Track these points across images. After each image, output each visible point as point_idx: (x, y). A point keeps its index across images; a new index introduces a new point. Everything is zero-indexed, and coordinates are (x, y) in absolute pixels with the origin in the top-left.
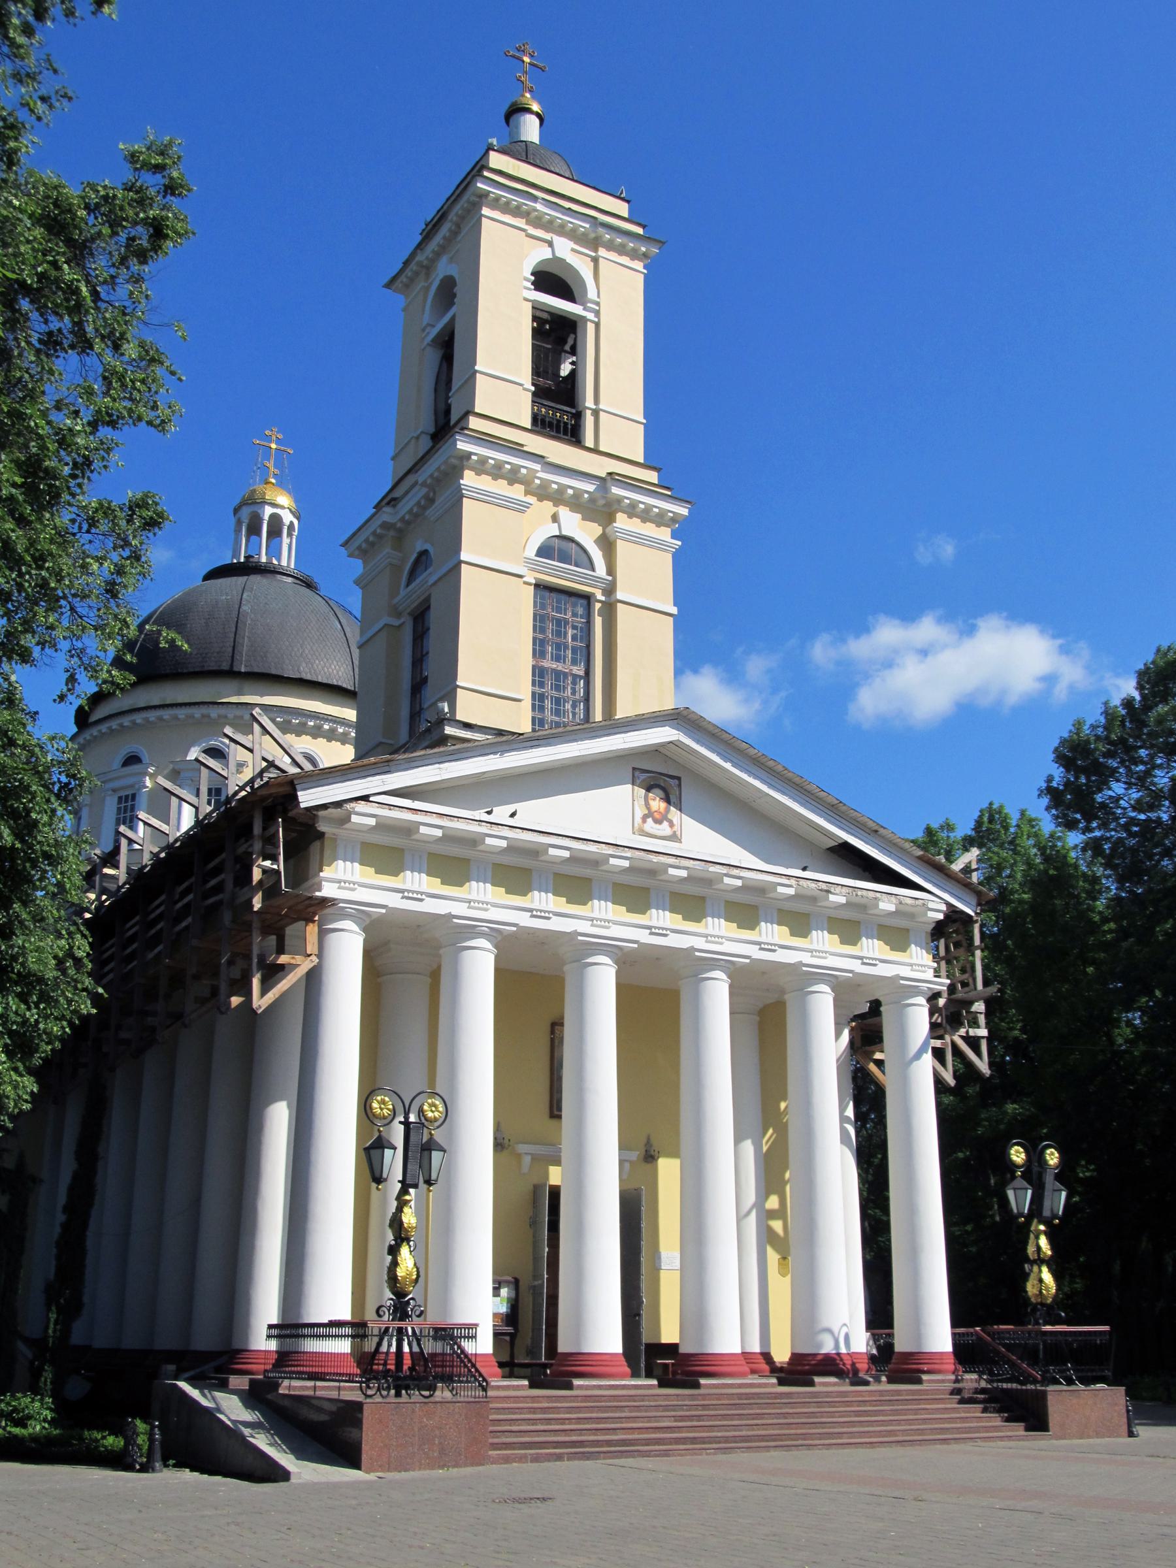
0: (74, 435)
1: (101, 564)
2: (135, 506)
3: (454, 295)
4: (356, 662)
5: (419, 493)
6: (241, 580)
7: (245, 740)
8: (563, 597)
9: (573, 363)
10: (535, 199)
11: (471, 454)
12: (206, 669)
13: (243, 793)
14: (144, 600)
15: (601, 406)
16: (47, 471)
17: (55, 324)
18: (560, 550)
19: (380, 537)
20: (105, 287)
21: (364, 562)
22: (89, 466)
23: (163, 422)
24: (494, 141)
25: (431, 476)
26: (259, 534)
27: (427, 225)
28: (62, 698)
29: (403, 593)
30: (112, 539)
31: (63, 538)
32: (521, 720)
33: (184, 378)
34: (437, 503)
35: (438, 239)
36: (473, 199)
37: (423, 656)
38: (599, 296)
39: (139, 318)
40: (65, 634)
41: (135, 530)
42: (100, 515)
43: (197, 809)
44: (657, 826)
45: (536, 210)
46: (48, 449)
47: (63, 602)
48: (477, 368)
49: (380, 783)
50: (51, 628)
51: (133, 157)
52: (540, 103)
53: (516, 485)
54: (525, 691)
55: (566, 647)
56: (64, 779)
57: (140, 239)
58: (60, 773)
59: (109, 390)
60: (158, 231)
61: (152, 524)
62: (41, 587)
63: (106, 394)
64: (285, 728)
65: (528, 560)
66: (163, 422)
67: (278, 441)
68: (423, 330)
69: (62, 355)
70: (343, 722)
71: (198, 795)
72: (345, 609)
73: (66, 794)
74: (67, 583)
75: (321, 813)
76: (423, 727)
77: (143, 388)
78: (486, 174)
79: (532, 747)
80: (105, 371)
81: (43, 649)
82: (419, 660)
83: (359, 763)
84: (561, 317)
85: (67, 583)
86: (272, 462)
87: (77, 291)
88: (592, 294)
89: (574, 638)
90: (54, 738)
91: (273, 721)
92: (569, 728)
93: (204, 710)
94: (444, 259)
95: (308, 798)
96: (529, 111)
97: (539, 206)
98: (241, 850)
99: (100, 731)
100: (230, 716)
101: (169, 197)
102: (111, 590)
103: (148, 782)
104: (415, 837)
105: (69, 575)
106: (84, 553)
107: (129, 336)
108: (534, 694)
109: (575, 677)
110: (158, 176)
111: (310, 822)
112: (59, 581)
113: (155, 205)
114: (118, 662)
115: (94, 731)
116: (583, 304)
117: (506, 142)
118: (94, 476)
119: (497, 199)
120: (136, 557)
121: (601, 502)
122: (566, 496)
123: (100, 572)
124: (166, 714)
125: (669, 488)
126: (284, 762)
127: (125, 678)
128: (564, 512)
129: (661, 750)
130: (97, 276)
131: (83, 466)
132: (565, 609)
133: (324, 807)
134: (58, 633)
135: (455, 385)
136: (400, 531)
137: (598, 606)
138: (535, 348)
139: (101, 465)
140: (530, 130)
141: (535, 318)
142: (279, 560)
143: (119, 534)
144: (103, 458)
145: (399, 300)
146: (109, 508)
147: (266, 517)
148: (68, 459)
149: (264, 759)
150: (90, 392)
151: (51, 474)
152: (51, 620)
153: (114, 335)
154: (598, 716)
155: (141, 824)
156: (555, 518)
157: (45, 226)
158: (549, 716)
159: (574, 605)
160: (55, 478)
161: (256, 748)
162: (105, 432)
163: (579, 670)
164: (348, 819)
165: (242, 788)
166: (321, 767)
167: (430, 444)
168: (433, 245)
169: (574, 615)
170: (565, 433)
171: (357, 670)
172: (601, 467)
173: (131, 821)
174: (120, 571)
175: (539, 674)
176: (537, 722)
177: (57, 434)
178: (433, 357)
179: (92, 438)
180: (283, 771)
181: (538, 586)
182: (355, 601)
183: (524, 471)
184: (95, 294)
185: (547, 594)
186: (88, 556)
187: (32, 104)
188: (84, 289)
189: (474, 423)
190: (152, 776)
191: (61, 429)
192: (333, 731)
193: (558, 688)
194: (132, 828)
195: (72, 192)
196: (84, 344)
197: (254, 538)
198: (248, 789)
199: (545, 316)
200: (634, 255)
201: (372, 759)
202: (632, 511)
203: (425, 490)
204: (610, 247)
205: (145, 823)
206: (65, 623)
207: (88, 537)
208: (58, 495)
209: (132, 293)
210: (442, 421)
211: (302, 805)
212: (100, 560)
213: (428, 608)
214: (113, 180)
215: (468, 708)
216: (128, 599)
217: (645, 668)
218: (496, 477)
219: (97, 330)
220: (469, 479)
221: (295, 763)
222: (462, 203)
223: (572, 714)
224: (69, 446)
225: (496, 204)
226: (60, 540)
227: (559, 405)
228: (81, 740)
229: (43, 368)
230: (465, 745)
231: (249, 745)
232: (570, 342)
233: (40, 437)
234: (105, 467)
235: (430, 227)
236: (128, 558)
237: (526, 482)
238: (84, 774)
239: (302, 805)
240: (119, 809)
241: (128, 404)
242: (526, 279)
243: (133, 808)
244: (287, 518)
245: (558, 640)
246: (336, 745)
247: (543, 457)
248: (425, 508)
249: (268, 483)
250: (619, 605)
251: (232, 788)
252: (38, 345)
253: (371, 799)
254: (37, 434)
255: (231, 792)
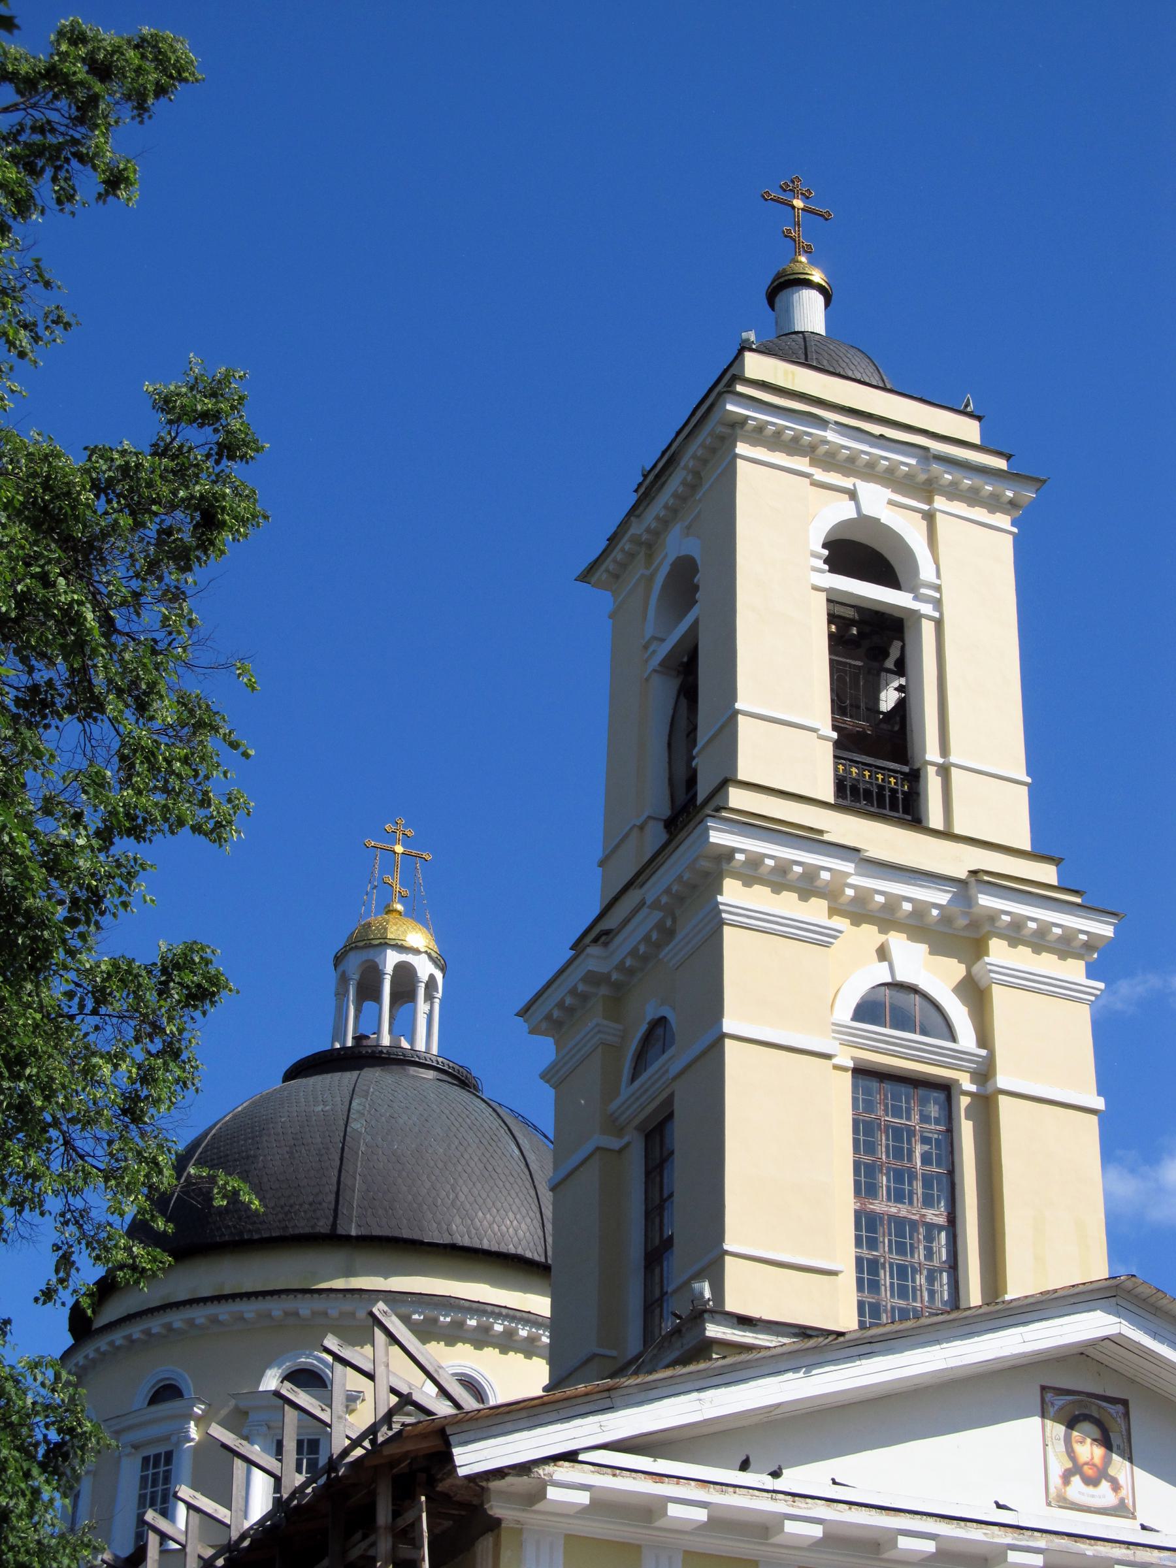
0: (73, 853)
1: (116, 1066)
2: (171, 967)
3: (696, 588)
4: (548, 1213)
5: (645, 923)
6: (349, 1077)
7: (360, 1355)
8: (903, 1089)
9: (900, 689)
10: (823, 423)
11: (733, 851)
12: (291, 1231)
13: (359, 1452)
14: (185, 1118)
15: (953, 759)
16: (28, 915)
17: (42, 675)
18: (893, 1008)
19: (584, 998)
20: (123, 610)
21: (557, 1043)
22: (97, 904)
23: (219, 825)
24: (751, 336)
25: (668, 891)
26: (378, 998)
27: (645, 476)
28: (48, 1295)
29: (626, 1091)
30: (132, 1023)
31: (54, 1024)
32: (839, 1310)
33: (252, 752)
34: (677, 940)
35: (665, 497)
36: (721, 429)
37: (663, 1201)
38: (938, 576)
39: (179, 658)
40: (57, 1186)
41: (171, 1009)
42: (114, 984)
43: (278, 1480)
44: (1091, 1490)
45: (826, 442)
46: (31, 880)
47: (53, 1133)
48: (738, 706)
49: (596, 1428)
50: (34, 1176)
51: (166, 403)
52: (825, 271)
53: (813, 900)
54: (842, 1253)
55: (912, 1176)
56: (54, 1436)
57: (179, 530)
58: (47, 1426)
59: (130, 777)
60: (209, 518)
61: (200, 996)
62: (19, 1109)
63: (126, 782)
64: (425, 1333)
65: (838, 1028)
66: (219, 825)
67: (407, 841)
68: (646, 647)
69: (54, 722)
70: (528, 1318)
71: (279, 1451)
72: (526, 1122)
73: (56, 1460)
74: (61, 1100)
75: (495, 1485)
76: (668, 1325)
77: (186, 771)
78: (740, 388)
79: (860, 1356)
80: (123, 745)
81: (20, 1212)
82: (657, 1206)
83: (558, 1394)
84: (877, 613)
85: (61, 1100)
86: (398, 876)
87: (76, 620)
88: (926, 572)
89: (926, 1159)
90: (37, 1365)
91: (406, 1320)
92: (924, 1321)
93: (288, 1303)
94: (676, 530)
95: (471, 1458)
96: (808, 284)
97: (831, 436)
98: (355, 1553)
99: (112, 1344)
100: (333, 1313)
101: (225, 461)
102: (132, 1110)
103: (194, 1432)
104: (660, 1523)
105: (64, 1087)
106: (87, 1048)
107: (162, 688)
108: (859, 1260)
109: (931, 1227)
110: (208, 430)
111: (475, 1501)
112: (47, 1098)
113: (204, 475)
114: (139, 1230)
115: (102, 1343)
116: (913, 589)
117: (771, 336)
118: (106, 920)
119: (761, 428)
120: (172, 1052)
121: (962, 922)
122: (899, 915)
123: (116, 1078)
124: (223, 1311)
125: (1078, 892)
126: (426, 1394)
127: (154, 1260)
128: (898, 942)
129: (1091, 1352)
130: (110, 595)
131: (88, 905)
132: (908, 1111)
133: (499, 1473)
134: (45, 1185)
135: (702, 737)
136: (618, 986)
137: (965, 1101)
138: (833, 664)
139: (117, 901)
140: (810, 313)
141: (832, 618)
142: (412, 1041)
143: (146, 1015)
144: (121, 891)
145: (600, 600)
146: (129, 972)
147: (389, 969)
148: (63, 894)
149: (393, 1391)
150: (99, 783)
151: (36, 920)
152: (33, 1162)
153: (138, 688)
154: (974, 1296)
155: (181, 1510)
156: (883, 953)
157: (27, 520)
158: (888, 1299)
159: (923, 1102)
160: (42, 925)
161: (380, 1373)
162: (124, 846)
163: (936, 1215)
164: (541, 1495)
165: (356, 1443)
166: (492, 1402)
167: (664, 837)
168: (657, 508)
169: (925, 1118)
170: (894, 807)
171: (549, 1227)
172: (957, 861)
173: (165, 1500)
174: (147, 1077)
175: (867, 1226)
176: (868, 1311)
177: (46, 853)
178: (663, 691)
179: (102, 857)
180: (428, 1413)
181: (861, 1072)
182: (541, 1104)
183: (825, 876)
184: (107, 623)
185: (874, 1085)
186: (94, 1054)
187: (11, 333)
188: (90, 616)
189: (737, 798)
190: (199, 1420)
191: (53, 845)
192: (509, 1334)
193: (901, 1249)
194: (167, 1513)
195: (71, 463)
196: (89, 705)
197: (368, 1005)
198: (366, 1444)
199: (850, 613)
200: (994, 504)
201: (581, 1388)
202: (1015, 934)
203: (657, 915)
204: (953, 493)
205: (190, 1506)
206: (56, 1166)
207: (95, 1020)
208: (47, 954)
209: (166, 618)
210: (682, 797)
211: (462, 1472)
212: (114, 1059)
213: (671, 1116)
214: (134, 439)
215: (745, 1289)
216: (162, 1123)
217: (1054, 1207)
218: (777, 888)
219: (110, 681)
220: (732, 894)
221: (444, 1393)
222: (703, 436)
223: (926, 1292)
224: (64, 872)
225: (759, 436)
226: (50, 1028)
227: (882, 763)
228: (79, 1358)
229: (24, 747)
230: (744, 1357)
231: (367, 1367)
232: (894, 653)
233: (17, 859)
234: (125, 905)
235: (651, 477)
236: (157, 1056)
237: (831, 894)
238: (88, 1426)
239: (462, 1472)
240: (144, 1479)
241: (160, 798)
242: (815, 555)
243: (167, 1479)
244: (425, 969)
245: (898, 1164)
246: (515, 1359)
247: (857, 850)
248: (658, 946)
249: (389, 911)
250: (1001, 1098)
251: (339, 1443)
252: (14, 709)
253: (581, 1457)
254: (13, 855)
255: (336, 1450)
